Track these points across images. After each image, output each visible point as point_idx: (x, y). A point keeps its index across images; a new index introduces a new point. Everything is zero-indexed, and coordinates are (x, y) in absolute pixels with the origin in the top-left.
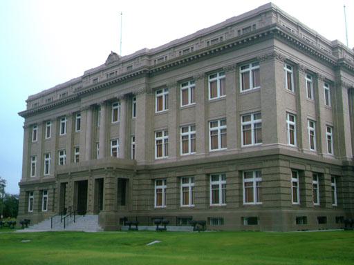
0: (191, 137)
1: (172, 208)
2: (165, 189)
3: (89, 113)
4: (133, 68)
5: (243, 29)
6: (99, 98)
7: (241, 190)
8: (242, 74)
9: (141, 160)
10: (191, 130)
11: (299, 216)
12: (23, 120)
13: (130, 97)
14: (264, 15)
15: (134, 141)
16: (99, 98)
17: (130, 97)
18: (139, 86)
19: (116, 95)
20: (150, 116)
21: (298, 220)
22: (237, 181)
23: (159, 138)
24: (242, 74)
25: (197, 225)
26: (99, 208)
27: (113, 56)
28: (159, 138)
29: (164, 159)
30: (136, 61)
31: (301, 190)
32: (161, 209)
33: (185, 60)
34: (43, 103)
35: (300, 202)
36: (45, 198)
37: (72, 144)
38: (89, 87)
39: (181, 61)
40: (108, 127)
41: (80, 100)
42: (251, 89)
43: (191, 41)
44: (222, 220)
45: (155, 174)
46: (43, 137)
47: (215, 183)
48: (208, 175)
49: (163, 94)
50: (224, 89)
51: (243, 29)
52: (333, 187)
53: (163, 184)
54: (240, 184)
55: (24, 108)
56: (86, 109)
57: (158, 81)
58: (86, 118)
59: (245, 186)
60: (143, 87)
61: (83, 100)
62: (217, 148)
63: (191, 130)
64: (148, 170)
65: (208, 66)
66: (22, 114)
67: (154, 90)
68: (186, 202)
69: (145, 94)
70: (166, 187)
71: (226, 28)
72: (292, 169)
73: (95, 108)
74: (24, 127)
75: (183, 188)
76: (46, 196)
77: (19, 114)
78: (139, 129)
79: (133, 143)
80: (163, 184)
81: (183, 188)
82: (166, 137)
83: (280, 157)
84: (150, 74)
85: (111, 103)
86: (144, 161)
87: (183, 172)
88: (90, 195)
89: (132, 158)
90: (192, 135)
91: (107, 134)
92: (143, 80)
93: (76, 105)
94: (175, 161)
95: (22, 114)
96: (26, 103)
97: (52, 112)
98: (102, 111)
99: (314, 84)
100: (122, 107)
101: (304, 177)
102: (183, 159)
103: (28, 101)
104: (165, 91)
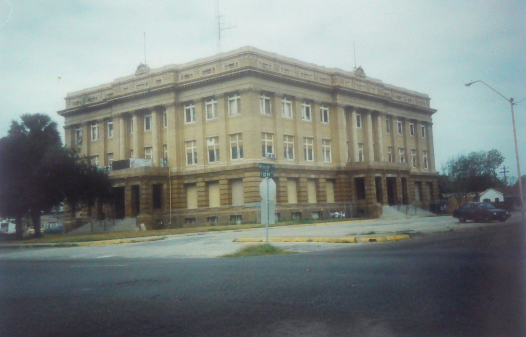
3: (121, 121)
4: (163, 83)
9: (174, 169)
13: (160, 110)
17: (160, 110)
18: (167, 100)
27: (360, 71)
40: (141, 133)
43: (192, 68)
45: (187, 182)
55: (63, 106)
57: (185, 97)
58: (119, 125)
61: (114, 108)
64: (179, 177)
69: (174, 107)
73: (127, 117)
78: (170, 136)
84: (177, 89)
85: (142, 113)
86: (176, 168)
87: (210, 179)
88: (127, 200)
91: (141, 141)
92: (173, 95)
93: (109, 111)
94: (203, 168)
96: (65, 101)
98: (134, 119)
100: (153, 116)
101: (300, 182)
103: (68, 99)
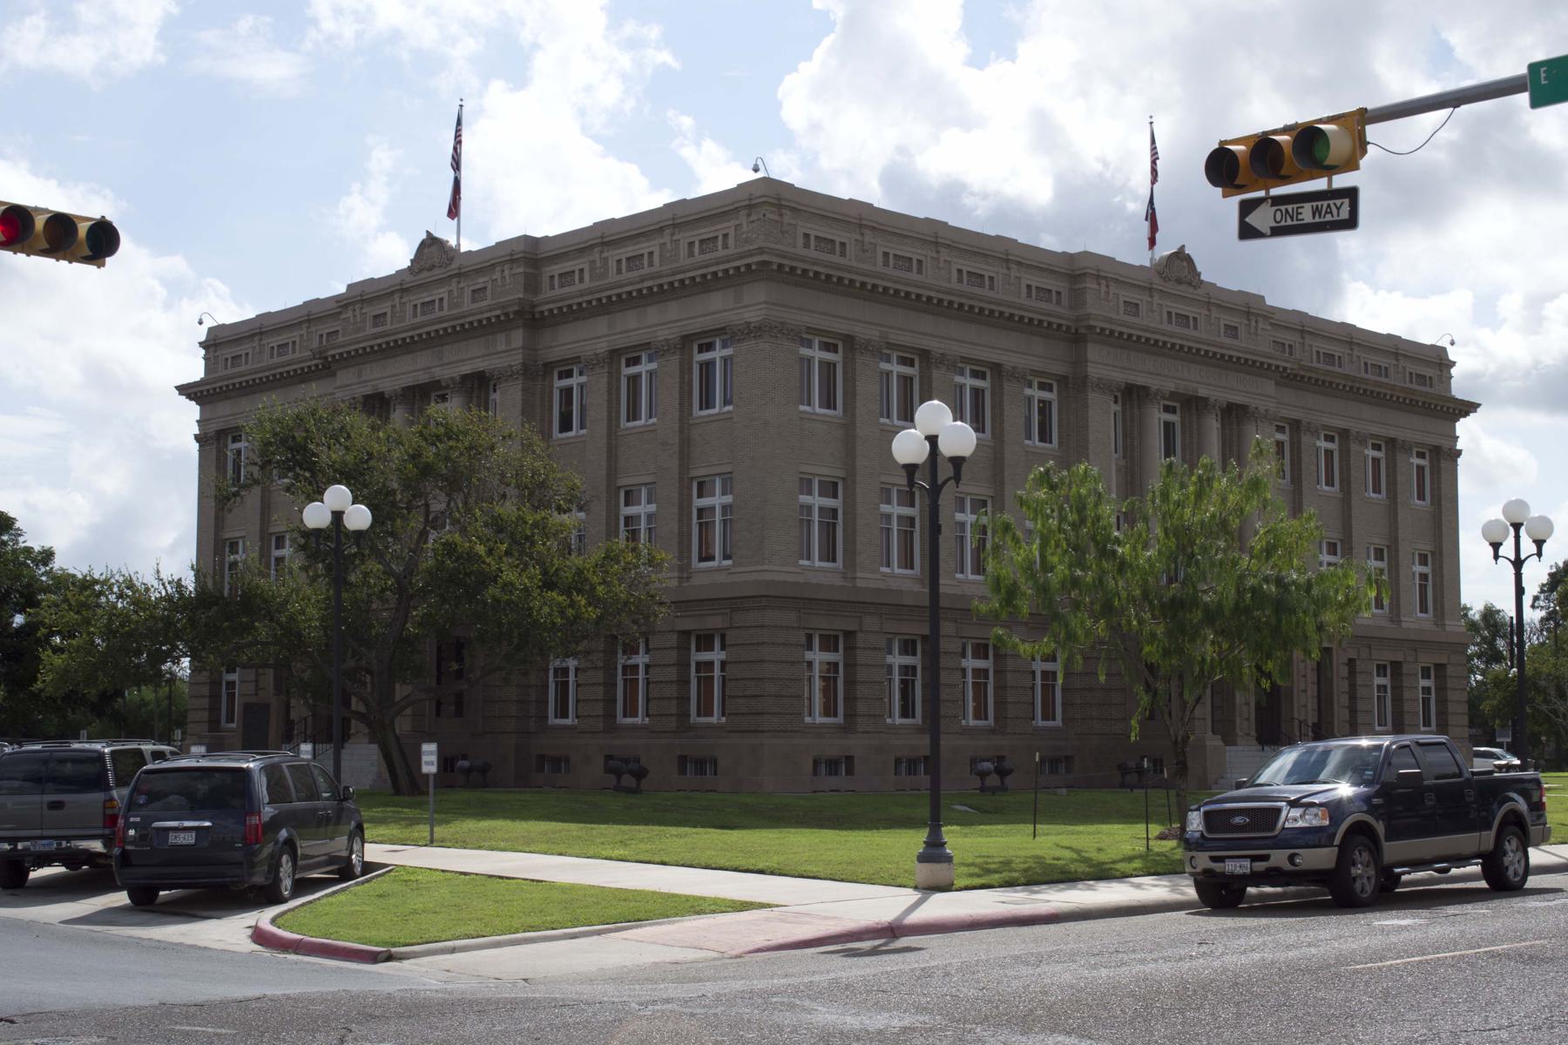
0: (649, 522)
2: (647, 667)
5: (702, 241)
10: (724, 493)
12: (192, 411)
14: (744, 212)
16: (392, 376)
21: (833, 765)
22: (672, 657)
29: (719, 570)
31: (850, 683)
32: (709, 726)
33: (507, 315)
34: (260, 361)
35: (845, 716)
36: (231, 684)
37: (612, 473)
38: (750, 254)
39: (507, 315)
41: (334, 375)
42: (642, 422)
44: (849, 760)
47: (705, 656)
49: (717, 354)
51: (702, 241)
55: (195, 370)
59: (698, 671)
60: (516, 360)
62: (712, 558)
66: (187, 390)
68: (630, 710)
70: (723, 656)
74: (197, 438)
75: (698, 664)
76: (234, 677)
77: (177, 388)
80: (642, 649)
81: (698, 664)
92: (518, 337)
95: (187, 390)
96: (203, 352)
97: (653, 315)
99: (993, 394)
102: (697, 581)
104: (724, 346)
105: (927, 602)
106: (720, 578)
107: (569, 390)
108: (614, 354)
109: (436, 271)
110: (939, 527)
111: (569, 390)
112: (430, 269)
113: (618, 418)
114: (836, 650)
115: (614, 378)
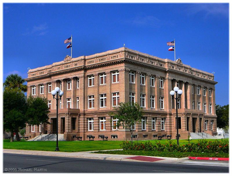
1: (108, 131)
2: (93, 122)
5: (114, 57)
6: (62, 77)
7: (99, 125)
8: (113, 75)
10: (105, 97)
11: (74, 135)
13: (76, 79)
15: (78, 99)
16: (62, 77)
19: (69, 77)
20: (85, 88)
22: (97, 121)
23: (114, 96)
24: (113, 75)
25: (79, 138)
26: (63, 131)
28: (114, 96)
29: (201, 105)
30: (79, 62)
39: (71, 70)
44: (117, 136)
46: (47, 92)
48: (99, 118)
50: (119, 80)
52: (211, 124)
53: (92, 120)
54: (99, 122)
56: (54, 82)
61: (52, 78)
63: (105, 97)
65: (101, 70)
67: (88, 76)
70: (93, 121)
71: (107, 55)
72: (98, 117)
79: (78, 100)
80: (92, 120)
82: (105, 97)
83: (83, 114)
85: (67, 80)
89: (60, 108)
90: (105, 99)
92: (83, 72)
102: (100, 109)
104: (105, 75)
105: (56, 113)
106: (105, 109)
107: (42, 88)
108: (99, 74)
109: (68, 61)
110: (57, 105)
111: (42, 88)
112: (67, 61)
113: (67, 89)
114: (154, 120)
115: (39, 88)
